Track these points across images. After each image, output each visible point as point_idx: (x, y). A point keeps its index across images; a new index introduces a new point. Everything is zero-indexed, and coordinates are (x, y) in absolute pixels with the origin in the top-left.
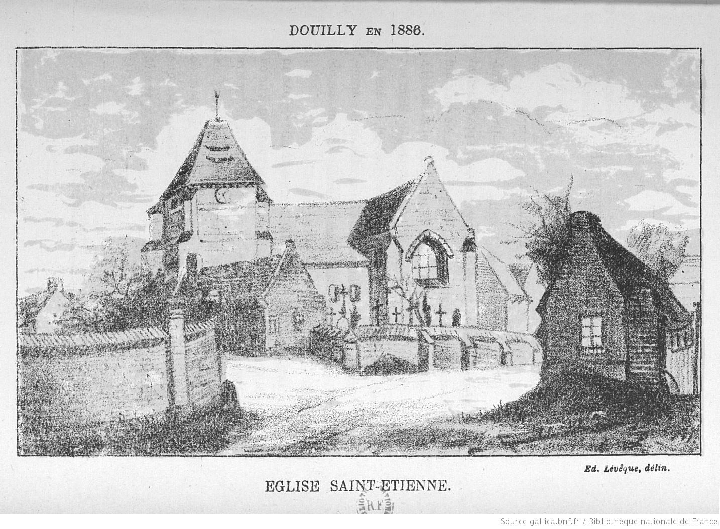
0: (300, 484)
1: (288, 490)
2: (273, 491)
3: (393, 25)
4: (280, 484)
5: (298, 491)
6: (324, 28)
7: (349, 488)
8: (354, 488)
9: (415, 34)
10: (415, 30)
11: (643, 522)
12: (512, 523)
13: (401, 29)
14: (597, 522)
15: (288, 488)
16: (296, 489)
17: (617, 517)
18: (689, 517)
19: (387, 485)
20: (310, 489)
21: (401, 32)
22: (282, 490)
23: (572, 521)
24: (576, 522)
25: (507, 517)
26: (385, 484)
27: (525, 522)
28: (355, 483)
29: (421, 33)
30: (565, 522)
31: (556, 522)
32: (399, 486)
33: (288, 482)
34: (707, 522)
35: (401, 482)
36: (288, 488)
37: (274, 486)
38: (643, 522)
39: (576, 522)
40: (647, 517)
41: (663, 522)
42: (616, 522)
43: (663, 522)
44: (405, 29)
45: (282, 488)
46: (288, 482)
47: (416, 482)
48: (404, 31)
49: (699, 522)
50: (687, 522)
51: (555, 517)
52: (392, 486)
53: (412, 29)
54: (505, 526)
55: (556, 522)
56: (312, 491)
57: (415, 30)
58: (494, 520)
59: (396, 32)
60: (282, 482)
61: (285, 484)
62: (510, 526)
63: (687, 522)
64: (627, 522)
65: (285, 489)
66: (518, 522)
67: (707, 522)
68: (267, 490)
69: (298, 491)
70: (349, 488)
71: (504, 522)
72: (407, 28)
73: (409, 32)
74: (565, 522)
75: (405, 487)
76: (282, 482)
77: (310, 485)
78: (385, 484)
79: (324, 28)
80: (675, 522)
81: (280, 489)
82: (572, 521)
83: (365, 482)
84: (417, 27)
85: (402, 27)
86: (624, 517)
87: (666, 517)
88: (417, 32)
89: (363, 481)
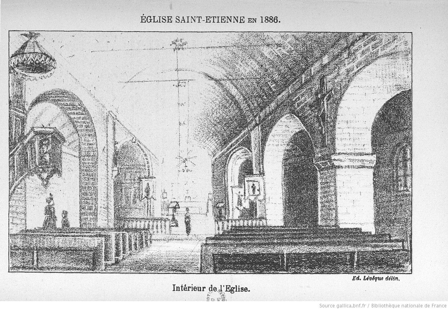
0: (161, 18)
1: (154, 22)
2: (145, 22)
3: (262, 17)
4: (149, 18)
5: (160, 22)
6: (218, 18)
7: (186, 21)
8: (190, 21)
9: (276, 23)
10: (274, 20)
11: (403, 306)
12: (326, 306)
13: (266, 19)
14: (376, 306)
15: (154, 21)
16: (159, 21)
17: (388, 303)
18: (430, 303)
19: (209, 19)
20: (167, 21)
21: (267, 21)
22: (151, 21)
23: (361, 306)
24: (364, 306)
25: (323, 303)
26: (208, 18)
27: (334, 306)
28: (190, 18)
29: (278, 22)
30: (357, 306)
31: (352, 306)
32: (216, 20)
33: (154, 17)
34: (440, 306)
35: (217, 18)
36: (154, 21)
37: (145, 19)
38: (403, 306)
39: (364, 306)
40: (405, 303)
41: (415, 306)
42: (387, 306)
43: (415, 306)
44: (269, 19)
45: (151, 20)
46: (154, 17)
47: (226, 18)
48: (268, 20)
49: (436, 306)
50: (429, 306)
51: (351, 303)
52: (212, 19)
53: (273, 19)
54: (322, 309)
55: (352, 306)
56: (168, 22)
57: (274, 19)
58: (315, 305)
59: (263, 21)
60: (150, 17)
61: (152, 18)
62: (325, 308)
63: (429, 306)
64: (394, 306)
65: (152, 21)
66: (329, 306)
67: (440, 306)
68: (142, 22)
69: (160, 22)
70: (186, 21)
71: (321, 306)
72: (270, 18)
73: (271, 21)
74: (357, 306)
75: (220, 21)
76: (150, 17)
77: (167, 19)
78: (208, 18)
79: (218, 18)
80: (422, 306)
81: (149, 21)
82: (361, 306)
83: (196, 17)
84: (276, 18)
85: (267, 18)
86: (392, 303)
87: (417, 303)
88: (276, 21)
89: (195, 17)
